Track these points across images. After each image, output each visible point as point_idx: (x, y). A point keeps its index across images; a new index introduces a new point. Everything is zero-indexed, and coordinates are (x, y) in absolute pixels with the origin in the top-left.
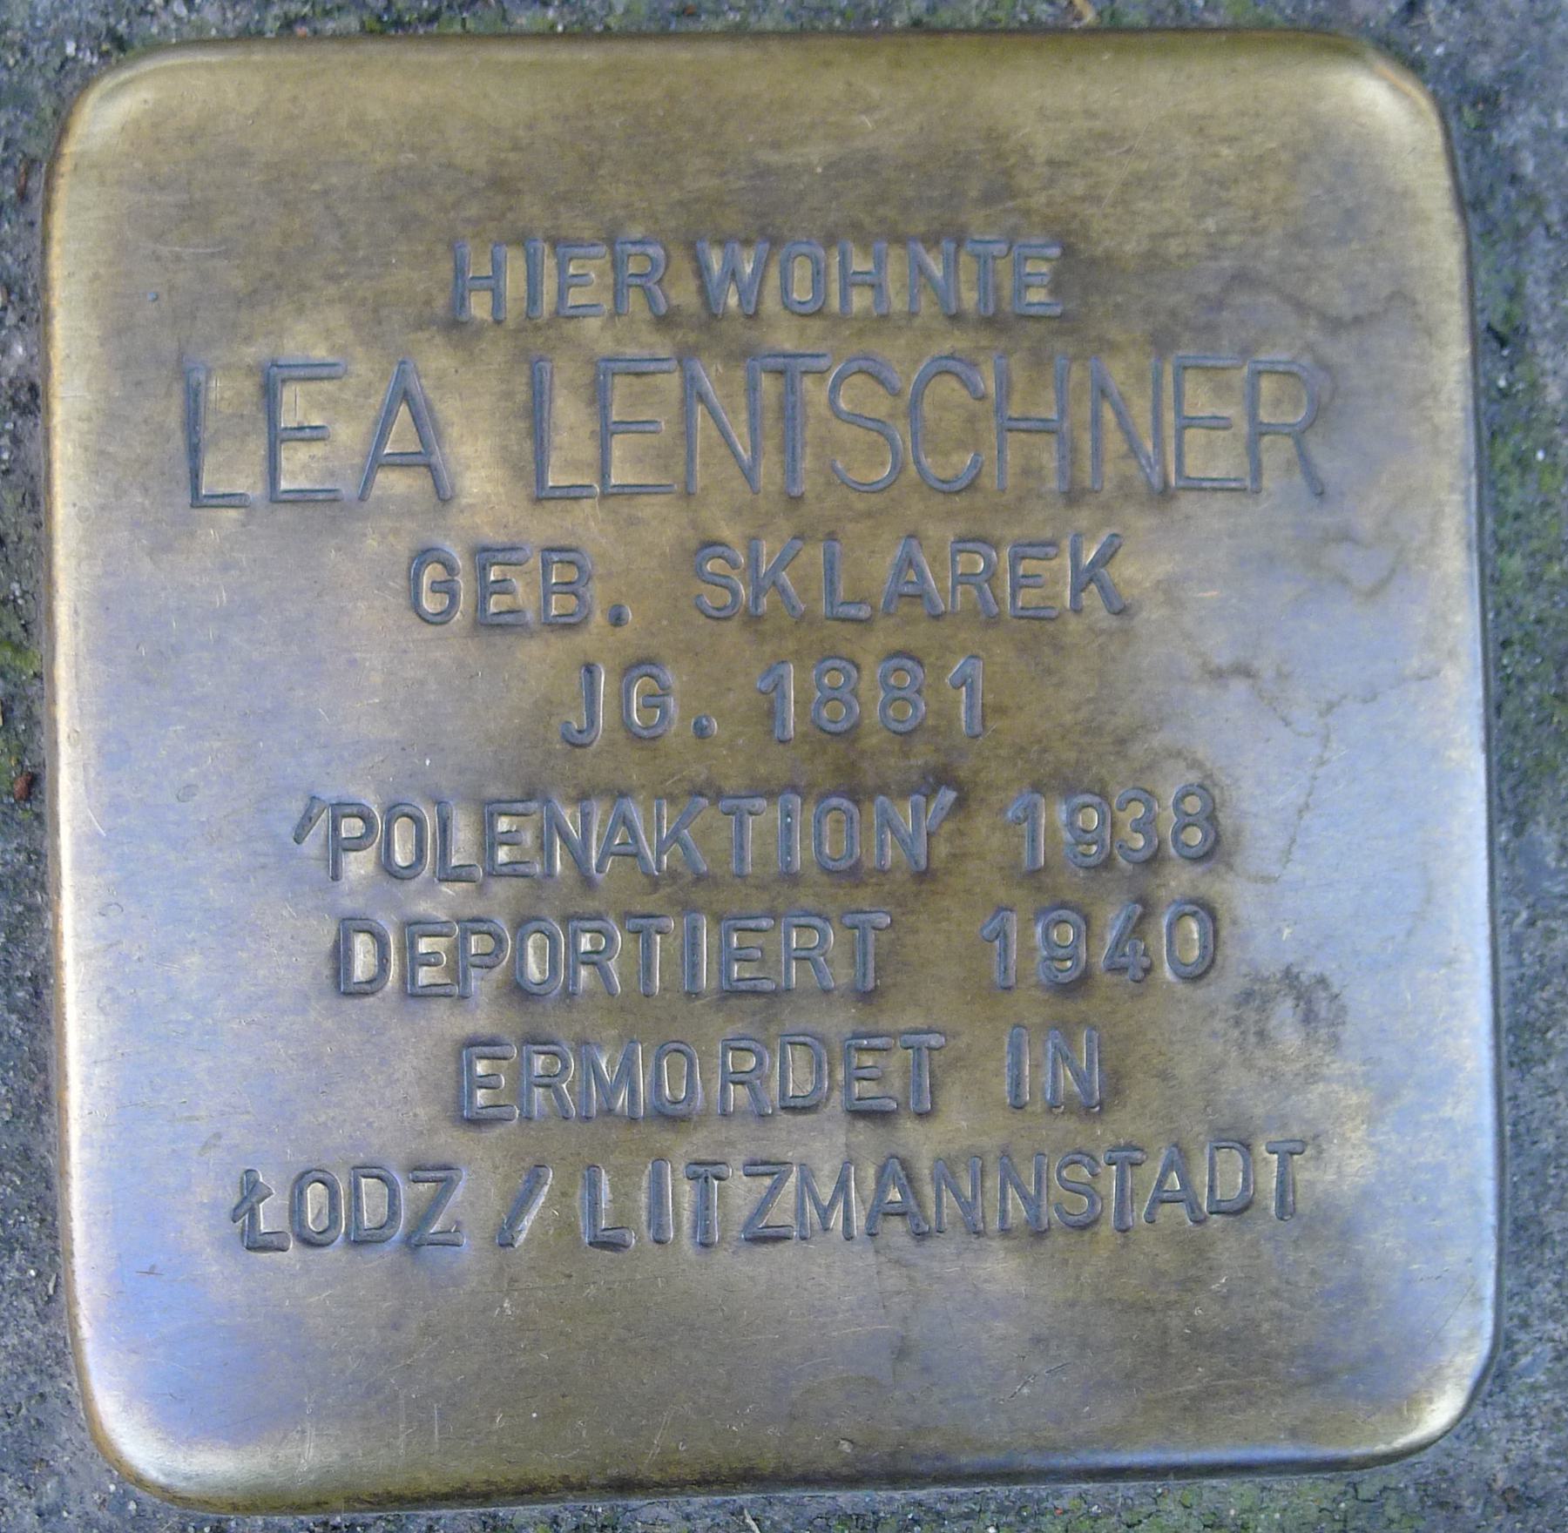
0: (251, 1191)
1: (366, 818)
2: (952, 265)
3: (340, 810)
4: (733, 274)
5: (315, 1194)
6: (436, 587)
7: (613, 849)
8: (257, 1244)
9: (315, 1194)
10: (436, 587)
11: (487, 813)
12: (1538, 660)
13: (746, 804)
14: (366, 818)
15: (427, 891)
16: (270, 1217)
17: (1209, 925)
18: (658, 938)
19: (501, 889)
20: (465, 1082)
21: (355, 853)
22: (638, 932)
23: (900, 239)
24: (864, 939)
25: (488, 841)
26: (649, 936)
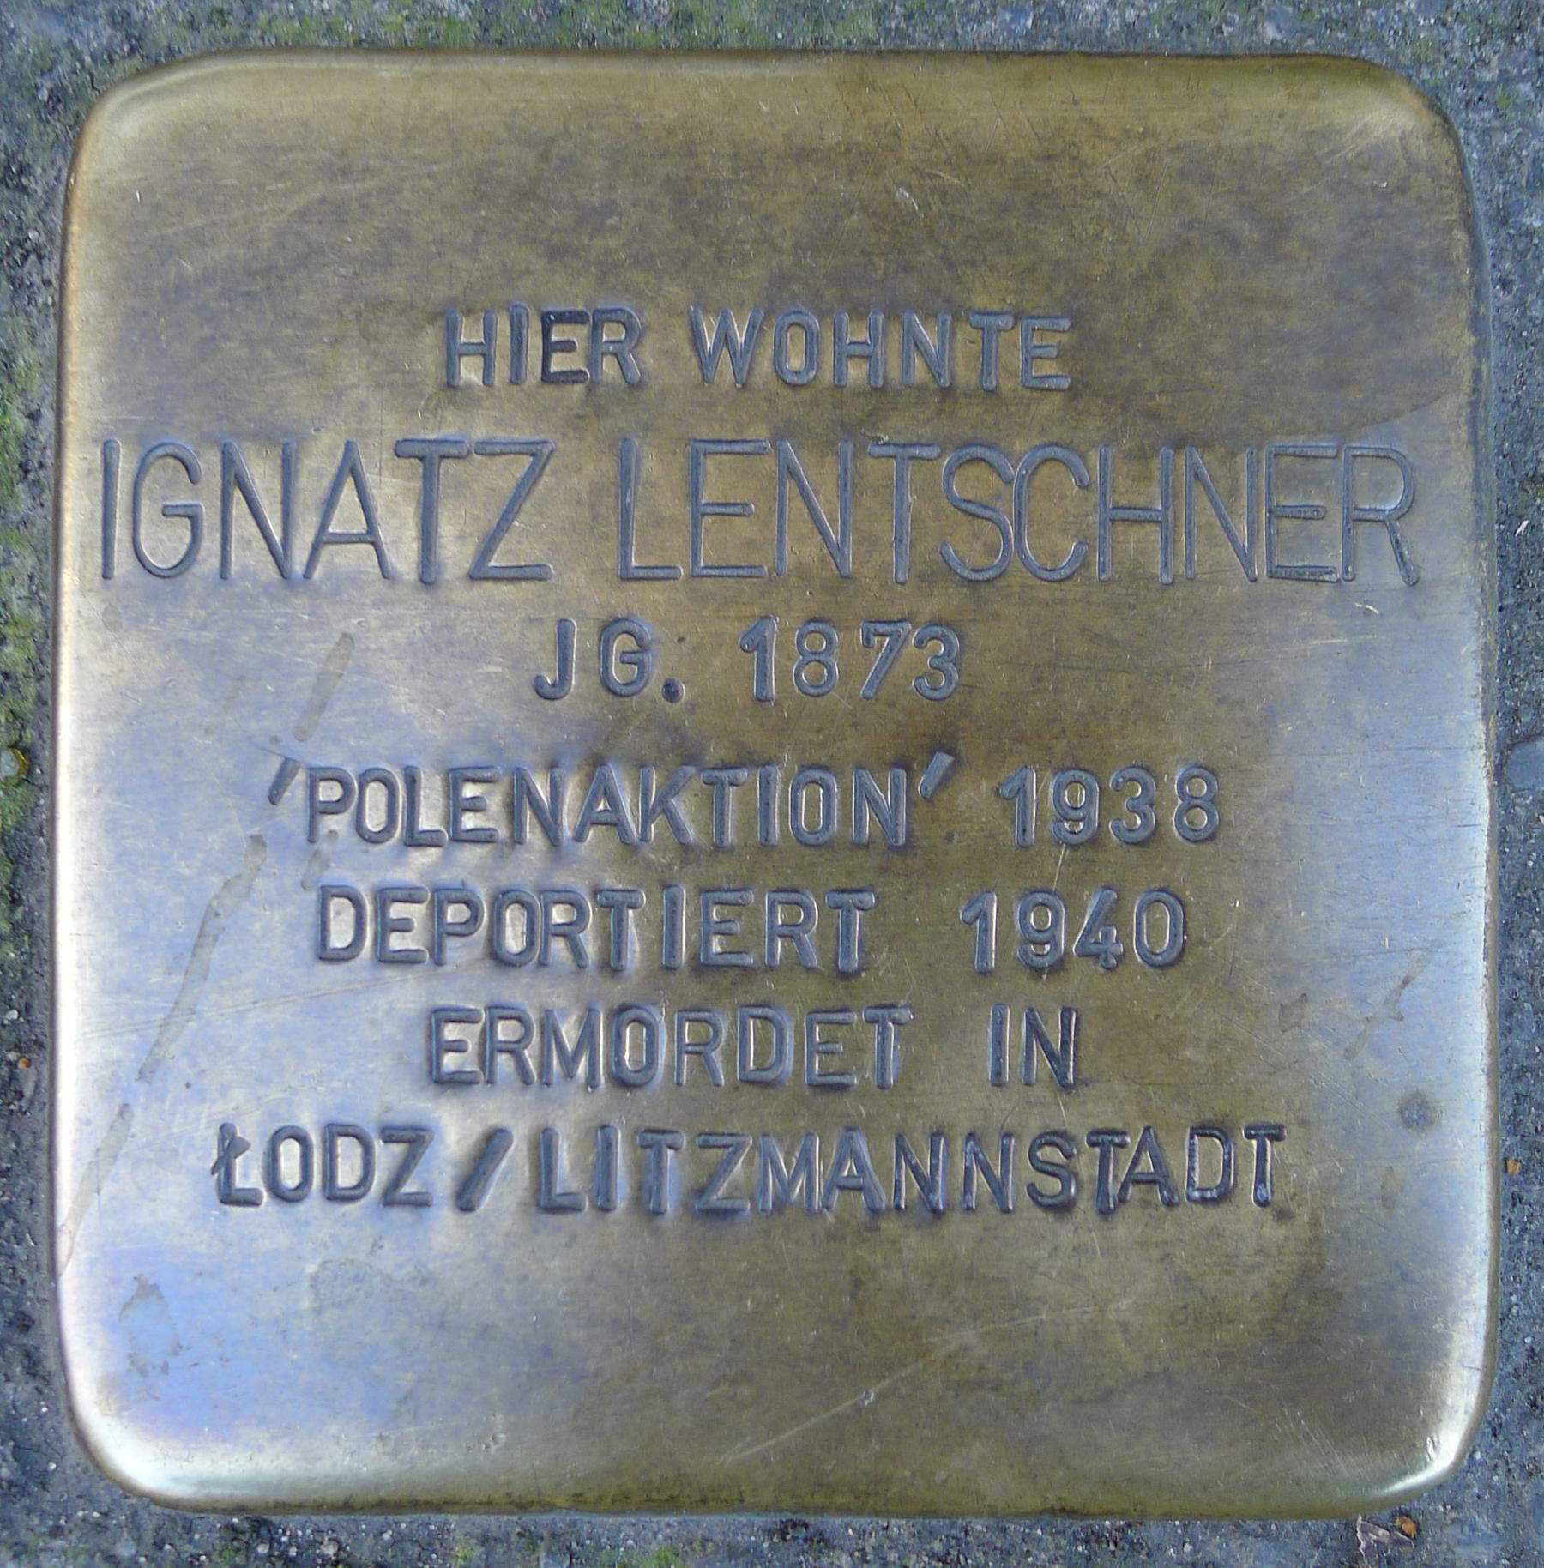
0: (230, 1145)
1: (344, 783)
2: (947, 337)
3: (316, 777)
4: (725, 339)
5: (290, 1153)
6: (626, 658)
7: (594, 817)
8: (230, 1197)
9: (290, 1153)
10: (626, 658)
11: (454, 779)
12: (434, 1556)
13: (725, 775)
14: (344, 783)
15: (398, 859)
16: (248, 1174)
17: (1047, 1201)
18: (631, 912)
19: (471, 855)
20: (437, 1047)
21: (335, 817)
22: (609, 907)
23: (893, 312)
24: (848, 924)
25: (456, 807)
26: (849, 911)
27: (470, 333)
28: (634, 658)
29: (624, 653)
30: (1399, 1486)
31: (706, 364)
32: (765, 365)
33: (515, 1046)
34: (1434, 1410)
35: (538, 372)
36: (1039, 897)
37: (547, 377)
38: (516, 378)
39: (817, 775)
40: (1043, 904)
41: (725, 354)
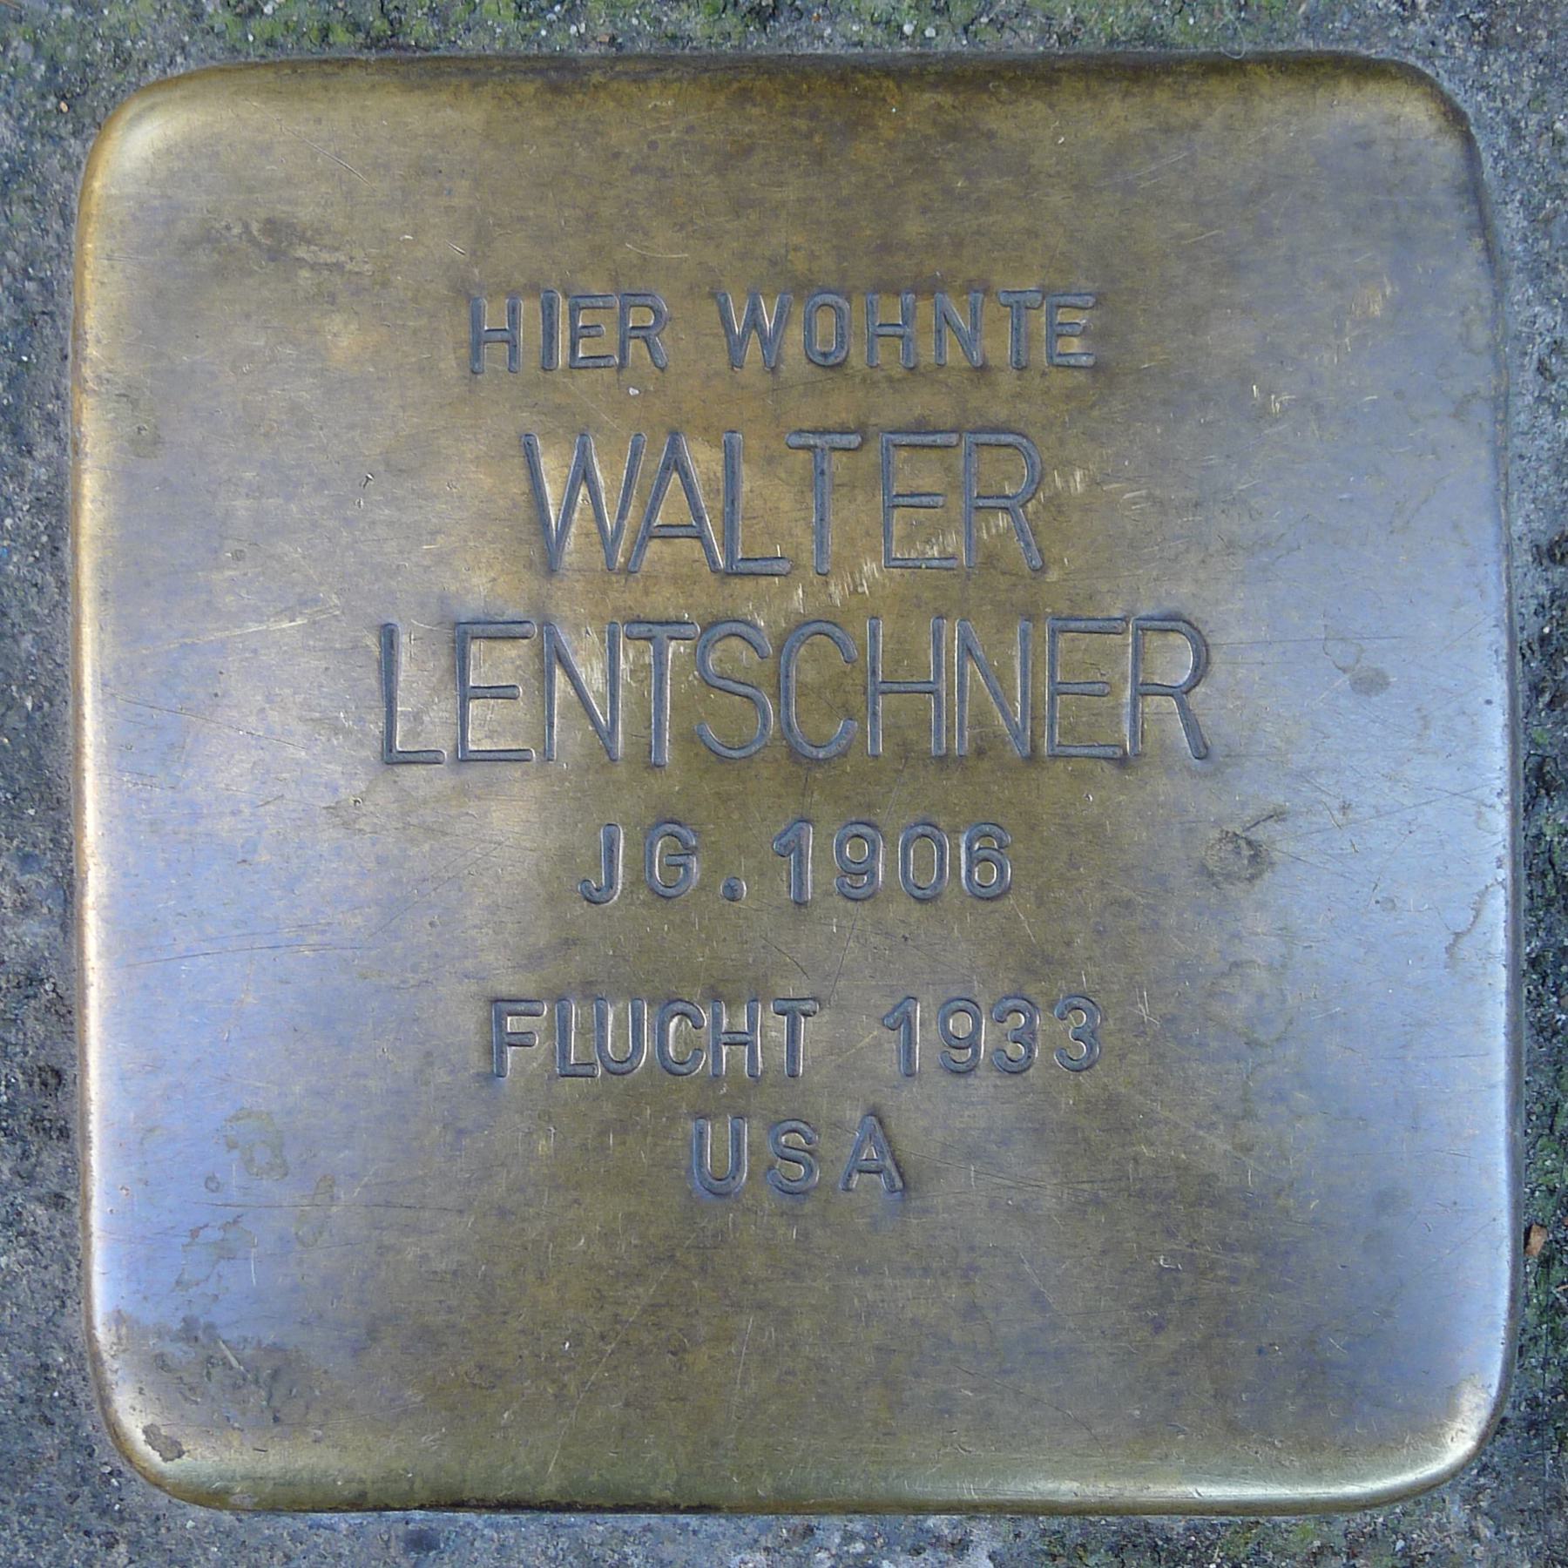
4: (754, 323)
28: (680, 860)
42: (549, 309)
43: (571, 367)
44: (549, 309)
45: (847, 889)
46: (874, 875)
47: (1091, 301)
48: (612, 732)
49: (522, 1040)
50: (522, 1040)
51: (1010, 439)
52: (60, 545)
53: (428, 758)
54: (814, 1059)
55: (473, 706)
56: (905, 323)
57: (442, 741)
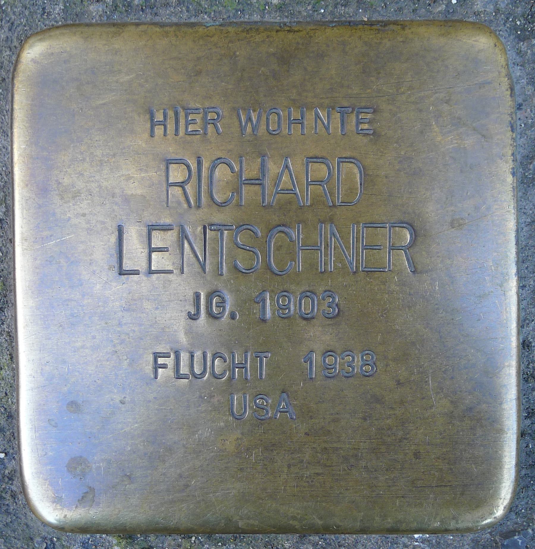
4: (249, 119)
27: (159, 117)
28: (221, 305)
29: (217, 303)
30: (484, 522)
31: (242, 129)
32: (263, 127)
33: (182, 184)
34: (494, 495)
35: (184, 131)
36: (367, 352)
37: (187, 133)
38: (177, 133)
39: (285, 293)
40: (368, 354)
41: (249, 125)
42: (176, 114)
43: (185, 134)
44: (176, 114)
45: (281, 315)
46: (289, 309)
47: (372, 110)
48: (205, 264)
49: (164, 366)
50: (164, 366)
51: (353, 161)
52: (116, 27)
53: (136, 272)
54: (269, 375)
55: (154, 255)
56: (302, 118)
57: (142, 266)
